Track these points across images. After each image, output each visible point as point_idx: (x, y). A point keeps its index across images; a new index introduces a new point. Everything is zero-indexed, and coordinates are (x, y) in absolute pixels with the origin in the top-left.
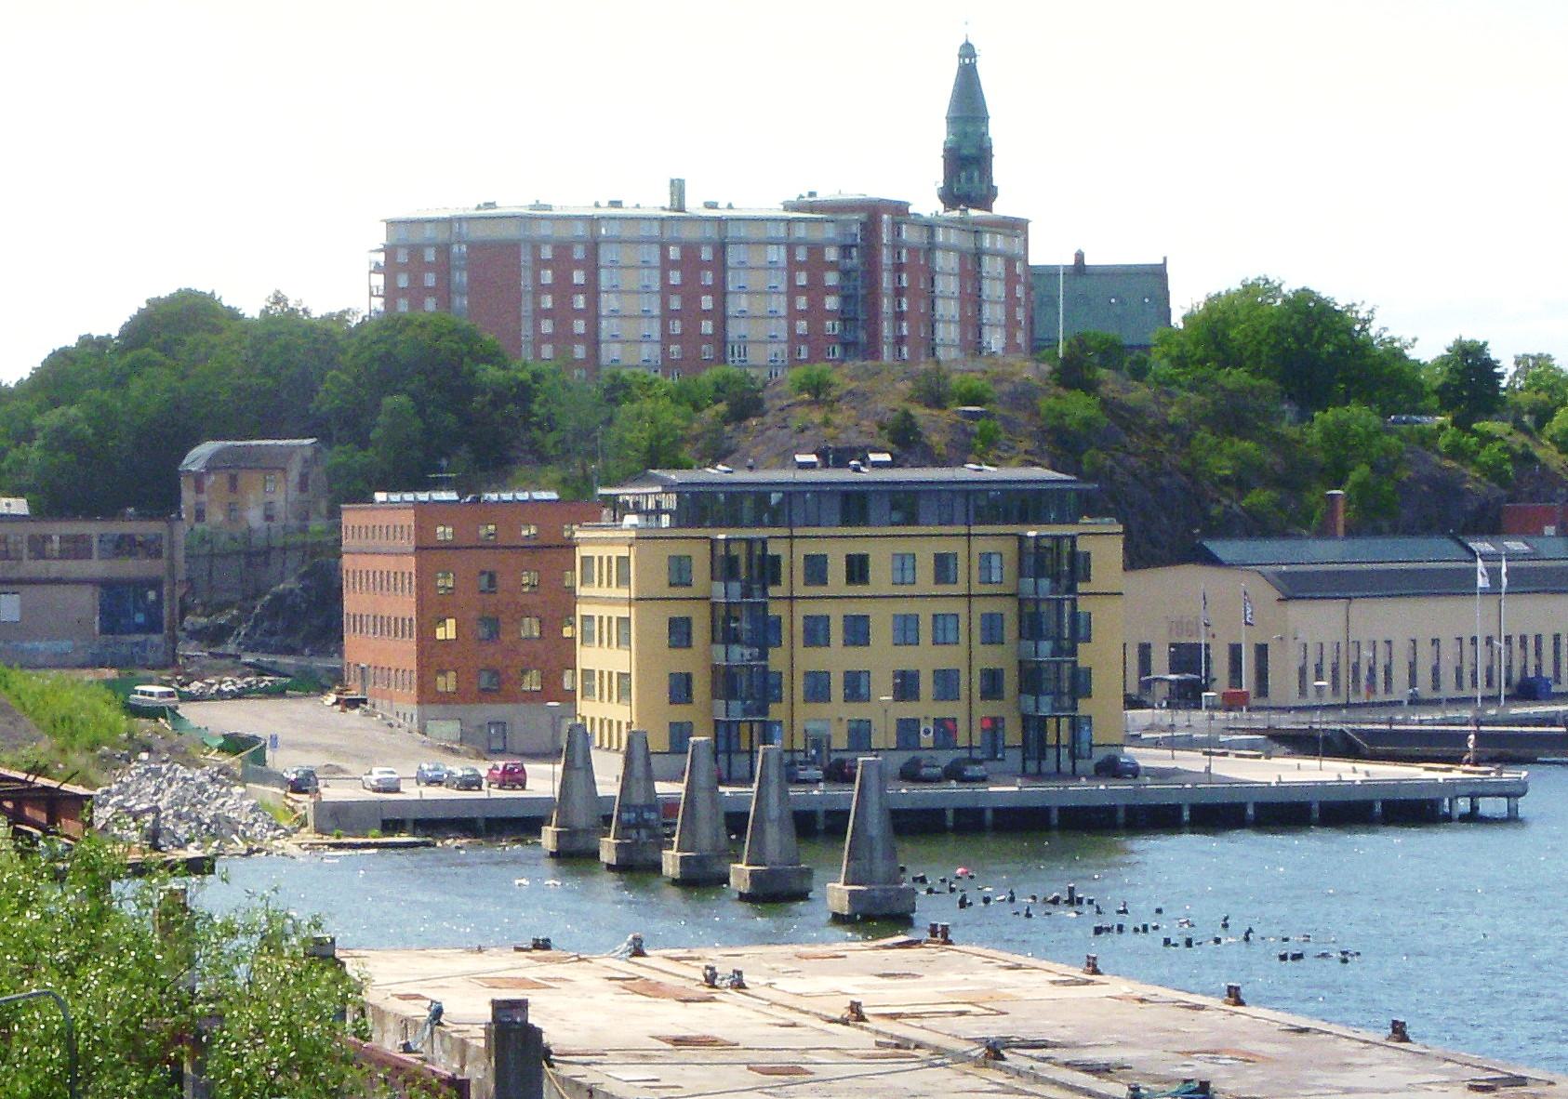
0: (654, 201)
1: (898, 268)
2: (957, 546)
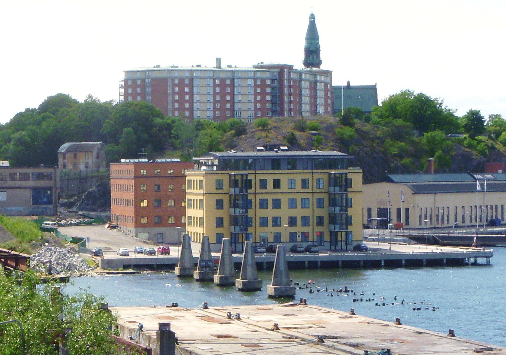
0: (211, 65)
1: (290, 87)
2: (309, 177)
